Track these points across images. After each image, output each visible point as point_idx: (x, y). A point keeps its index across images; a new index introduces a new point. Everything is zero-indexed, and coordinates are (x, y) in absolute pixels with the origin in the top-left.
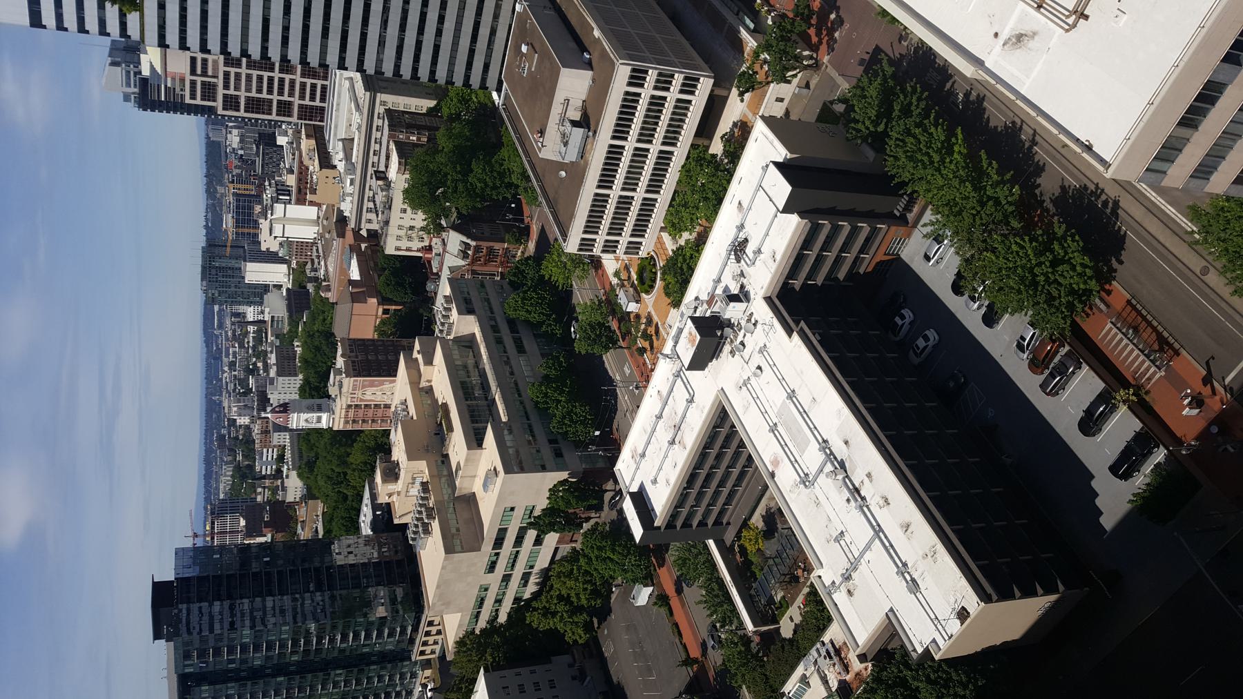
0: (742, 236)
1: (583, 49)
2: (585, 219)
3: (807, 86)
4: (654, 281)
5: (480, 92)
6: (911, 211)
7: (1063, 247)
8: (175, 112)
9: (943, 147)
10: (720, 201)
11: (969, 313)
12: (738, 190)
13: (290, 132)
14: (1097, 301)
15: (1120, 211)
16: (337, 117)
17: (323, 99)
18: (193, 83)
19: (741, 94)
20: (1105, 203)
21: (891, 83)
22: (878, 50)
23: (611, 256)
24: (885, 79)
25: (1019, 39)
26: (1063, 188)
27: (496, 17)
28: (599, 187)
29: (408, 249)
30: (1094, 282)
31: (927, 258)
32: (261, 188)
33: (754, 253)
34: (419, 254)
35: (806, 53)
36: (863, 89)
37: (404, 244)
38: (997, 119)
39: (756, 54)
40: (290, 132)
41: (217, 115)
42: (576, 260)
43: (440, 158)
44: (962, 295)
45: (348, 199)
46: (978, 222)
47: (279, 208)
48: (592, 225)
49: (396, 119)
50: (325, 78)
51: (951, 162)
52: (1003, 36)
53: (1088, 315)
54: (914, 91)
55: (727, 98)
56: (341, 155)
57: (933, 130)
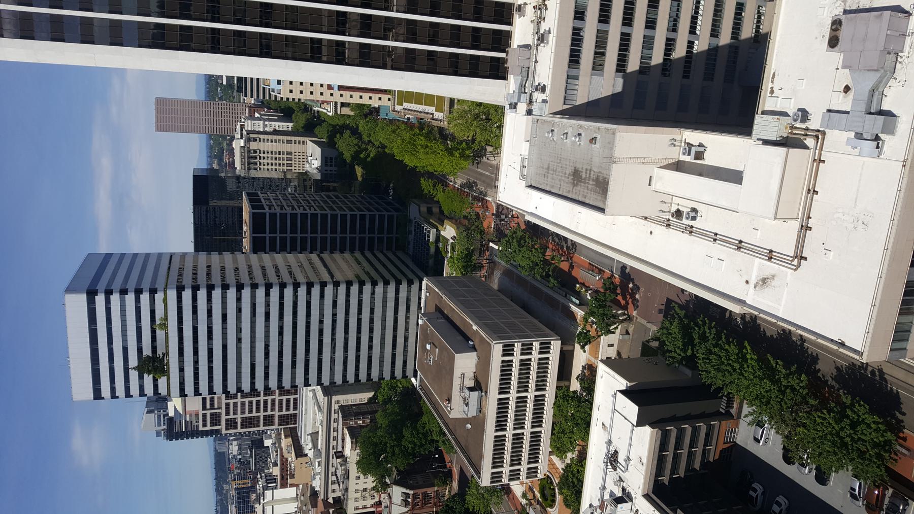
0: (612, 449)
1: (468, 339)
2: (491, 457)
3: (627, 333)
4: (554, 496)
5: (403, 381)
6: (732, 407)
7: (855, 413)
8: (192, 438)
9: (739, 358)
10: (588, 424)
11: (803, 476)
12: (600, 413)
13: (273, 436)
14: (898, 447)
15: (886, 376)
16: (306, 418)
17: (295, 408)
18: (204, 416)
19: (583, 347)
20: (873, 372)
21: (686, 321)
22: (669, 301)
23: (518, 482)
24: (681, 319)
25: (764, 281)
26: (837, 368)
27: (407, 329)
28: (497, 431)
29: (364, 507)
30: (889, 434)
31: (758, 441)
32: (255, 481)
33: (625, 461)
34: (373, 509)
35: (620, 312)
36: (667, 329)
37: (361, 504)
38: (771, 332)
39: (585, 319)
40: (273, 436)
41: (221, 434)
42: (491, 491)
43: (380, 433)
44: (794, 464)
45: (318, 477)
46: (785, 407)
47: (268, 493)
48: (497, 461)
49: (347, 411)
50: (296, 393)
51: (748, 367)
52: (753, 281)
53: (896, 461)
54: (704, 323)
55: (573, 351)
56: (310, 445)
57: (727, 347)
